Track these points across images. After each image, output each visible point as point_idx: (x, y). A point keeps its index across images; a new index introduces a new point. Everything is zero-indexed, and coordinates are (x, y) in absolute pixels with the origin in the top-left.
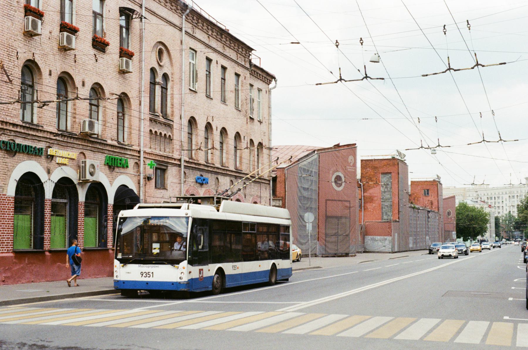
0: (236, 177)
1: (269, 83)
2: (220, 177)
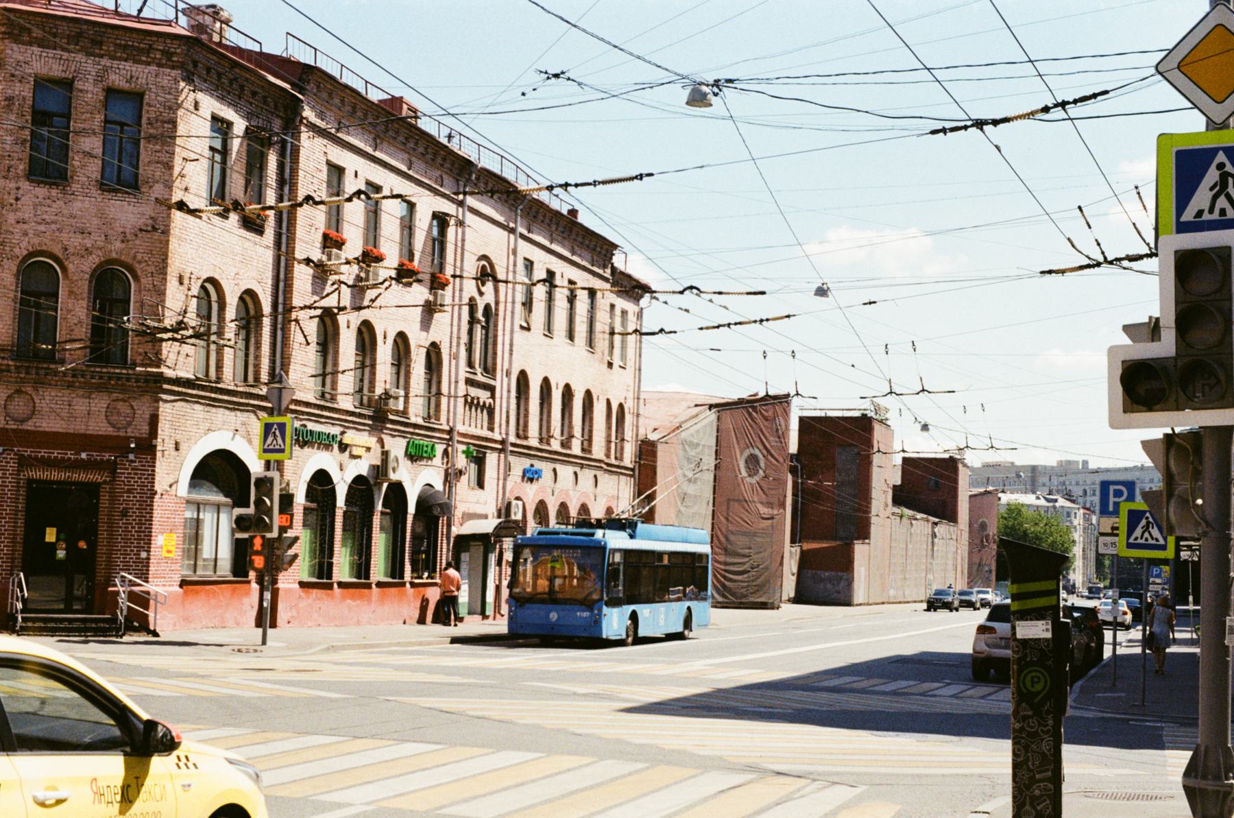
0: (582, 466)
1: (637, 299)
2: (559, 467)
